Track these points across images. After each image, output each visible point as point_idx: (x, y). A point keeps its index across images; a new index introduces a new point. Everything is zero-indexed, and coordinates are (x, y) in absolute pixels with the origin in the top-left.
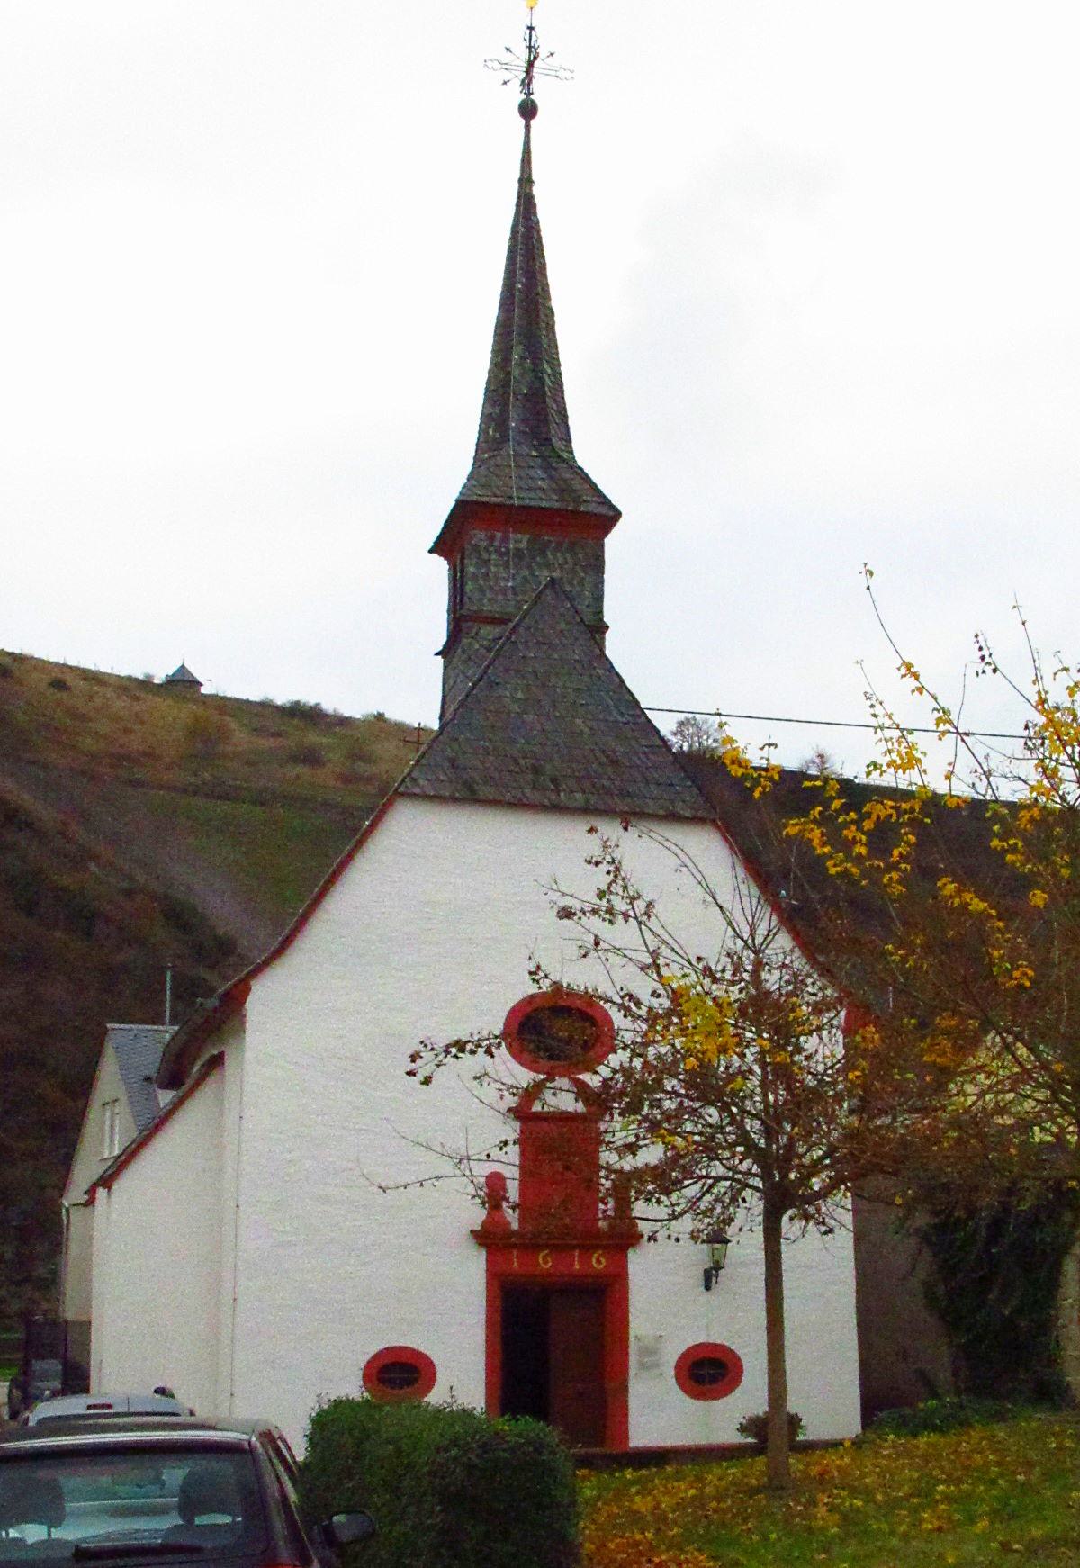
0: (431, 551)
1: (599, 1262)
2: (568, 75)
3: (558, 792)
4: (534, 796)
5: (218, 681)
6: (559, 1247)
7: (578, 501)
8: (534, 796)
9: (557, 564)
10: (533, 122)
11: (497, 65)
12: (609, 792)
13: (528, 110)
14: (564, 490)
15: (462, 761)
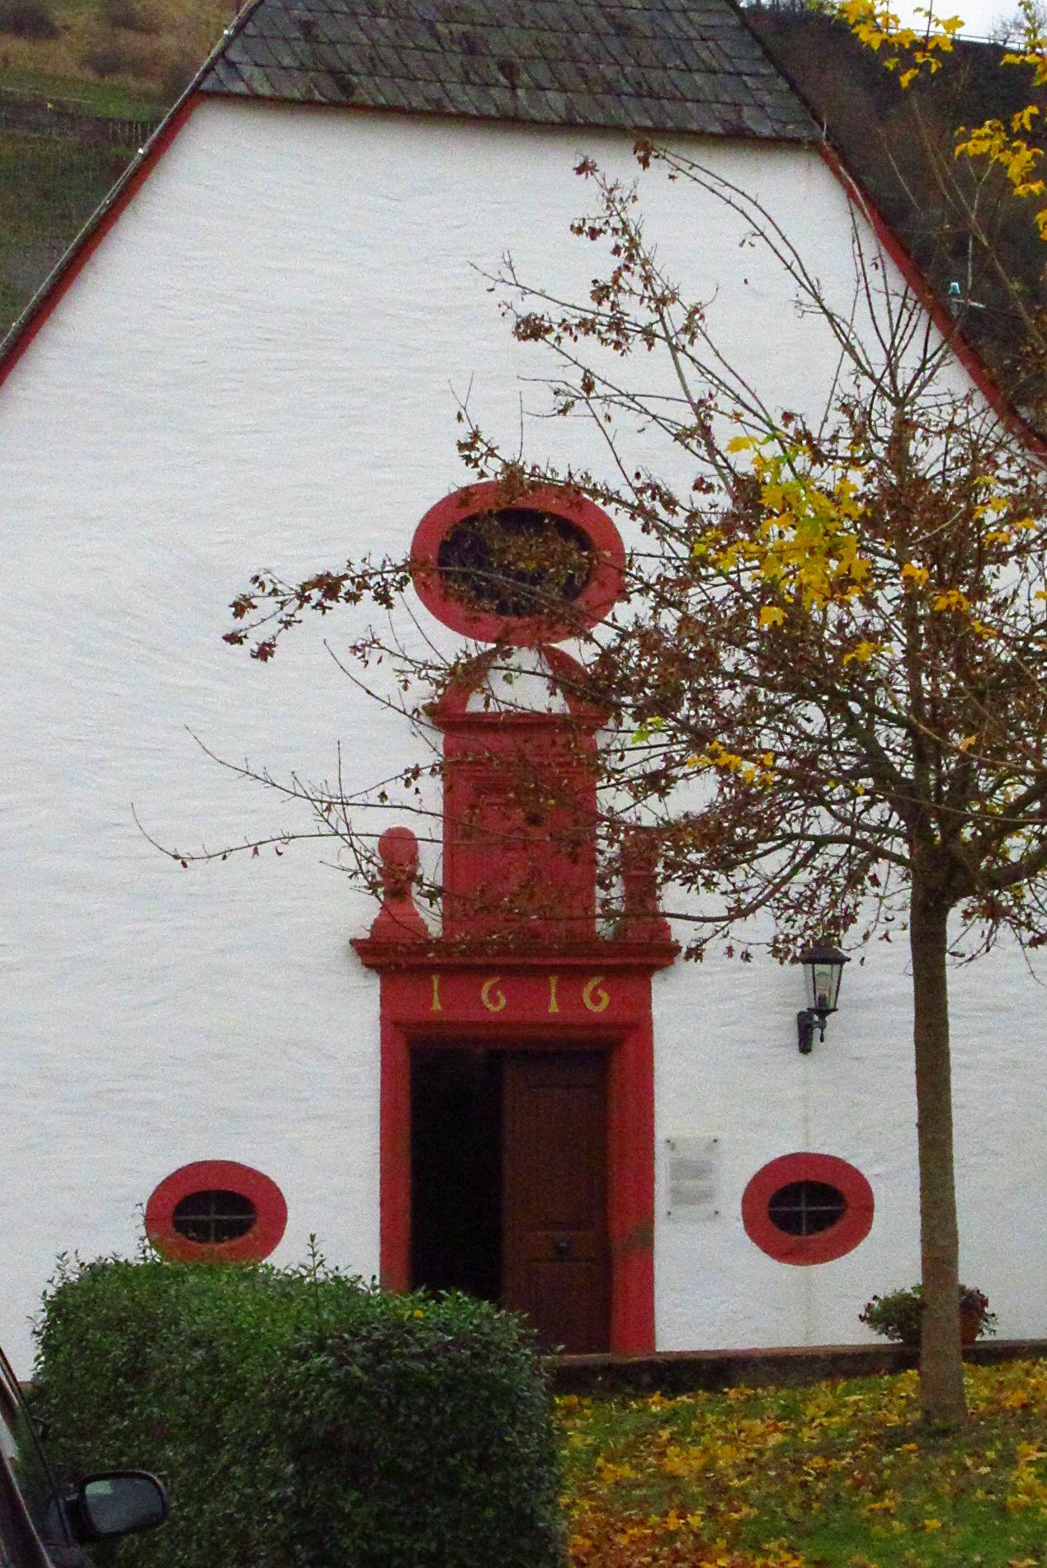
1: (595, 999)
8: (466, 98)
12: (610, 89)
15: (327, 30)
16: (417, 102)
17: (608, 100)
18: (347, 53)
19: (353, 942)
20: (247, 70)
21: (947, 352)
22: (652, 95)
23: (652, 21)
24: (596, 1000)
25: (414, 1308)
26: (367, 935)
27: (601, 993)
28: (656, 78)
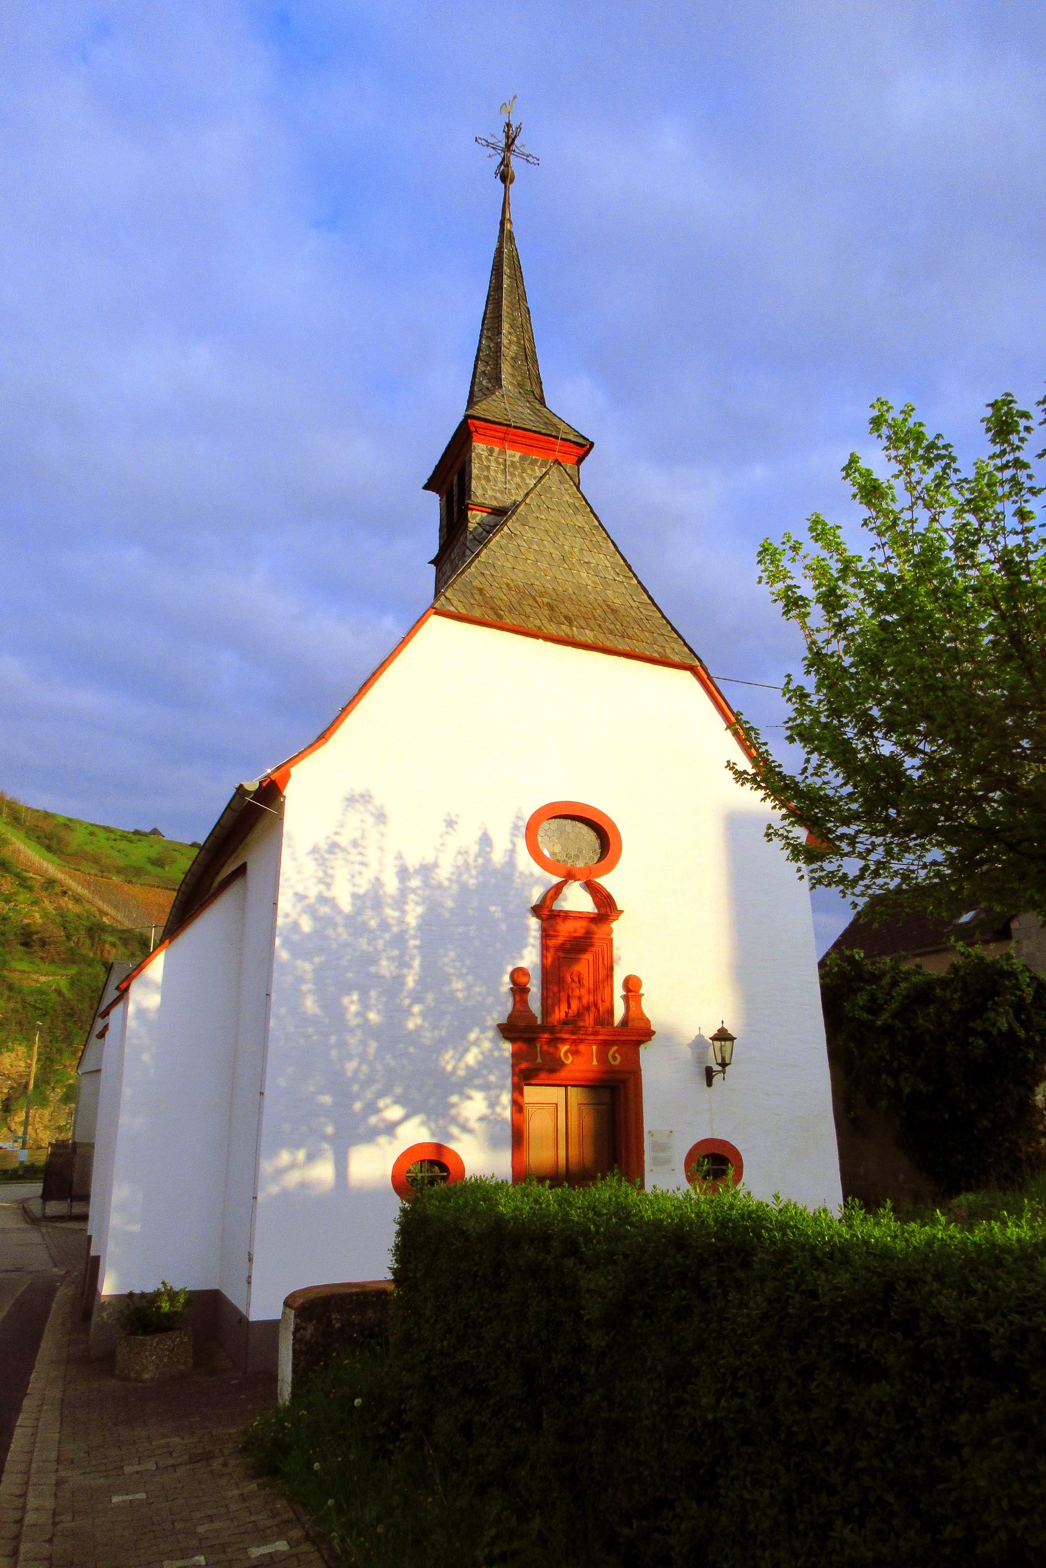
2: (536, 162)
10: (512, 187)
11: (485, 143)
12: (611, 632)
17: (611, 637)
18: (498, 602)
19: (499, 1025)
20: (455, 603)
22: (629, 637)
23: (625, 609)
24: (615, 1058)
26: (505, 1022)
27: (617, 1055)
28: (630, 632)
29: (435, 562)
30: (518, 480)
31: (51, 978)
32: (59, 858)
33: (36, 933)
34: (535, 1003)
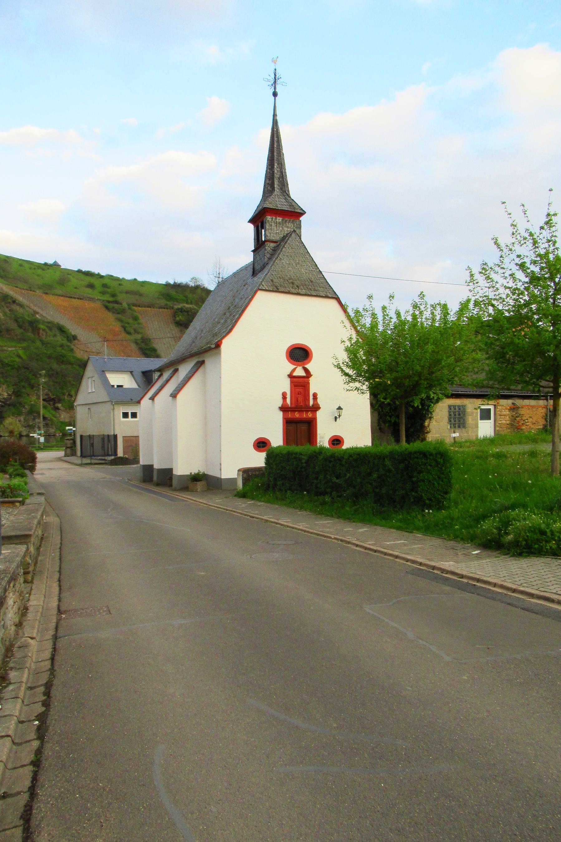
0: (248, 222)
1: (310, 415)
2: (286, 84)
3: (298, 289)
4: (293, 291)
5: (66, 264)
6: (300, 411)
7: (294, 208)
8: (293, 291)
9: (289, 227)
10: (277, 98)
11: (267, 80)
12: (311, 289)
13: (275, 94)
14: (291, 205)
15: (275, 280)
16: (287, 291)
18: (277, 284)
20: (265, 286)
21: (434, 320)
25: (287, 447)
28: (316, 288)
29: (253, 251)
30: (281, 228)
31: (13, 349)
32: (5, 280)
33: (3, 324)
34: (288, 401)
